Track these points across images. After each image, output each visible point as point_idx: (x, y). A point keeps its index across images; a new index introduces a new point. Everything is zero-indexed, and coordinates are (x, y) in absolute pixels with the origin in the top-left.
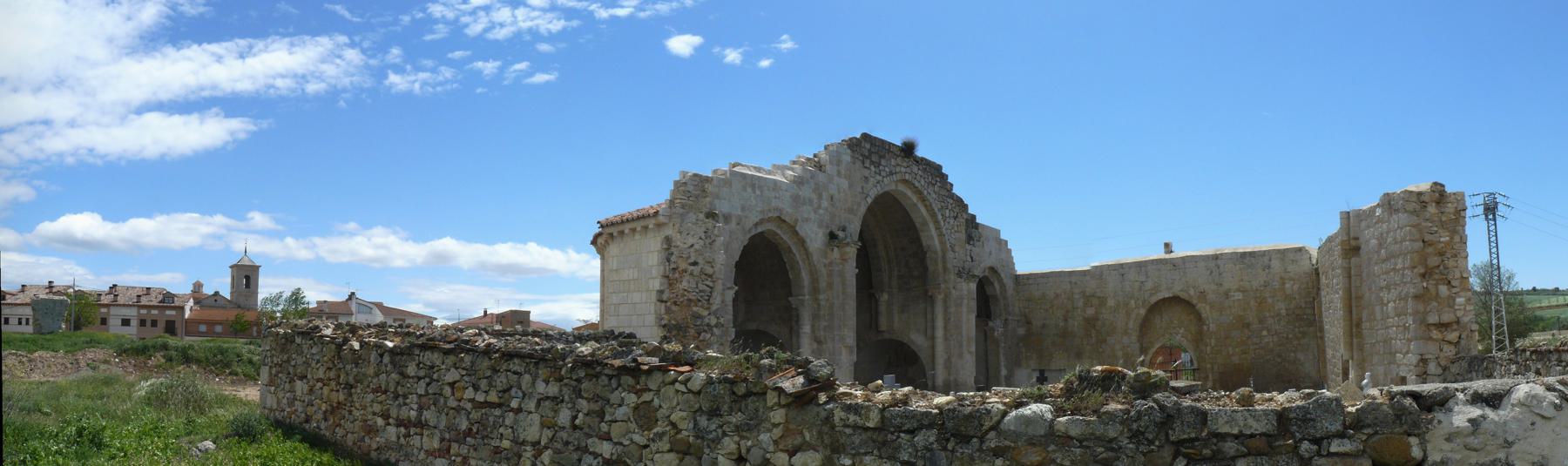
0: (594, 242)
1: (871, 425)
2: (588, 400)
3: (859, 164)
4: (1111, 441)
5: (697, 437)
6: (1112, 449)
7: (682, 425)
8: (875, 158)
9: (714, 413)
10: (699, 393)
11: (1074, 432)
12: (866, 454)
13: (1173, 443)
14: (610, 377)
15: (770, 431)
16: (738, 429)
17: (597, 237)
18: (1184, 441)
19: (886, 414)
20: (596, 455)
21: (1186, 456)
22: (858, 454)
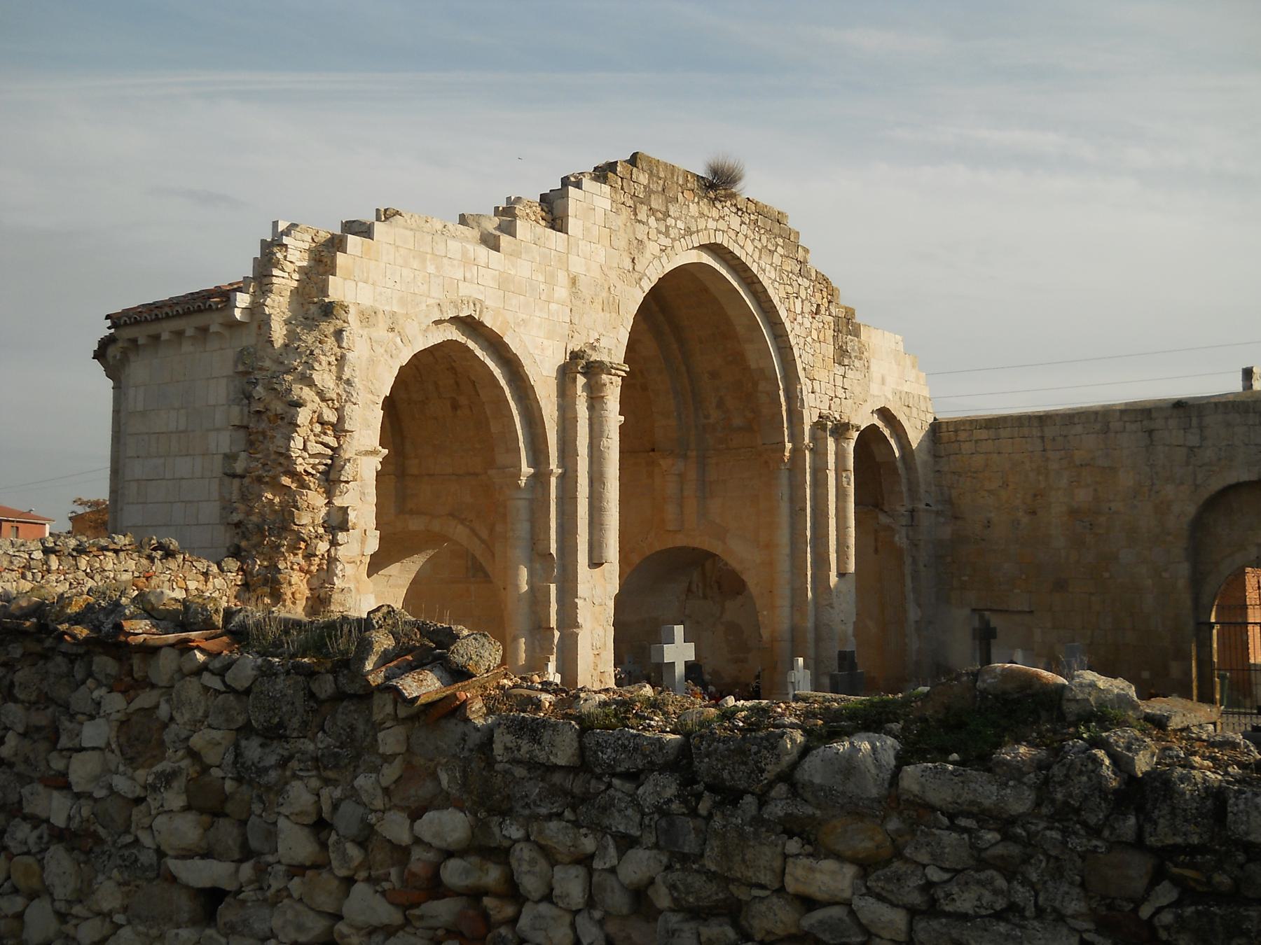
0: (100, 355)
1: (561, 760)
2: (30, 705)
3: (626, 213)
4: (1013, 821)
5: (239, 780)
6: (1015, 839)
7: (211, 757)
8: (656, 203)
9: (273, 733)
10: (248, 692)
11: (934, 797)
12: (550, 817)
13: (1152, 850)
14: (71, 659)
15: (376, 769)
16: (317, 762)
17: (105, 344)
18: (1176, 848)
19: (589, 741)
20: (36, 821)
21: (1177, 881)
22: (536, 817)
